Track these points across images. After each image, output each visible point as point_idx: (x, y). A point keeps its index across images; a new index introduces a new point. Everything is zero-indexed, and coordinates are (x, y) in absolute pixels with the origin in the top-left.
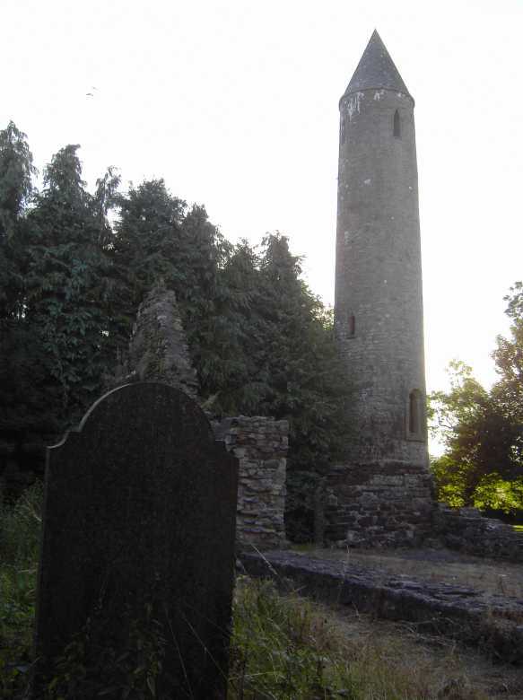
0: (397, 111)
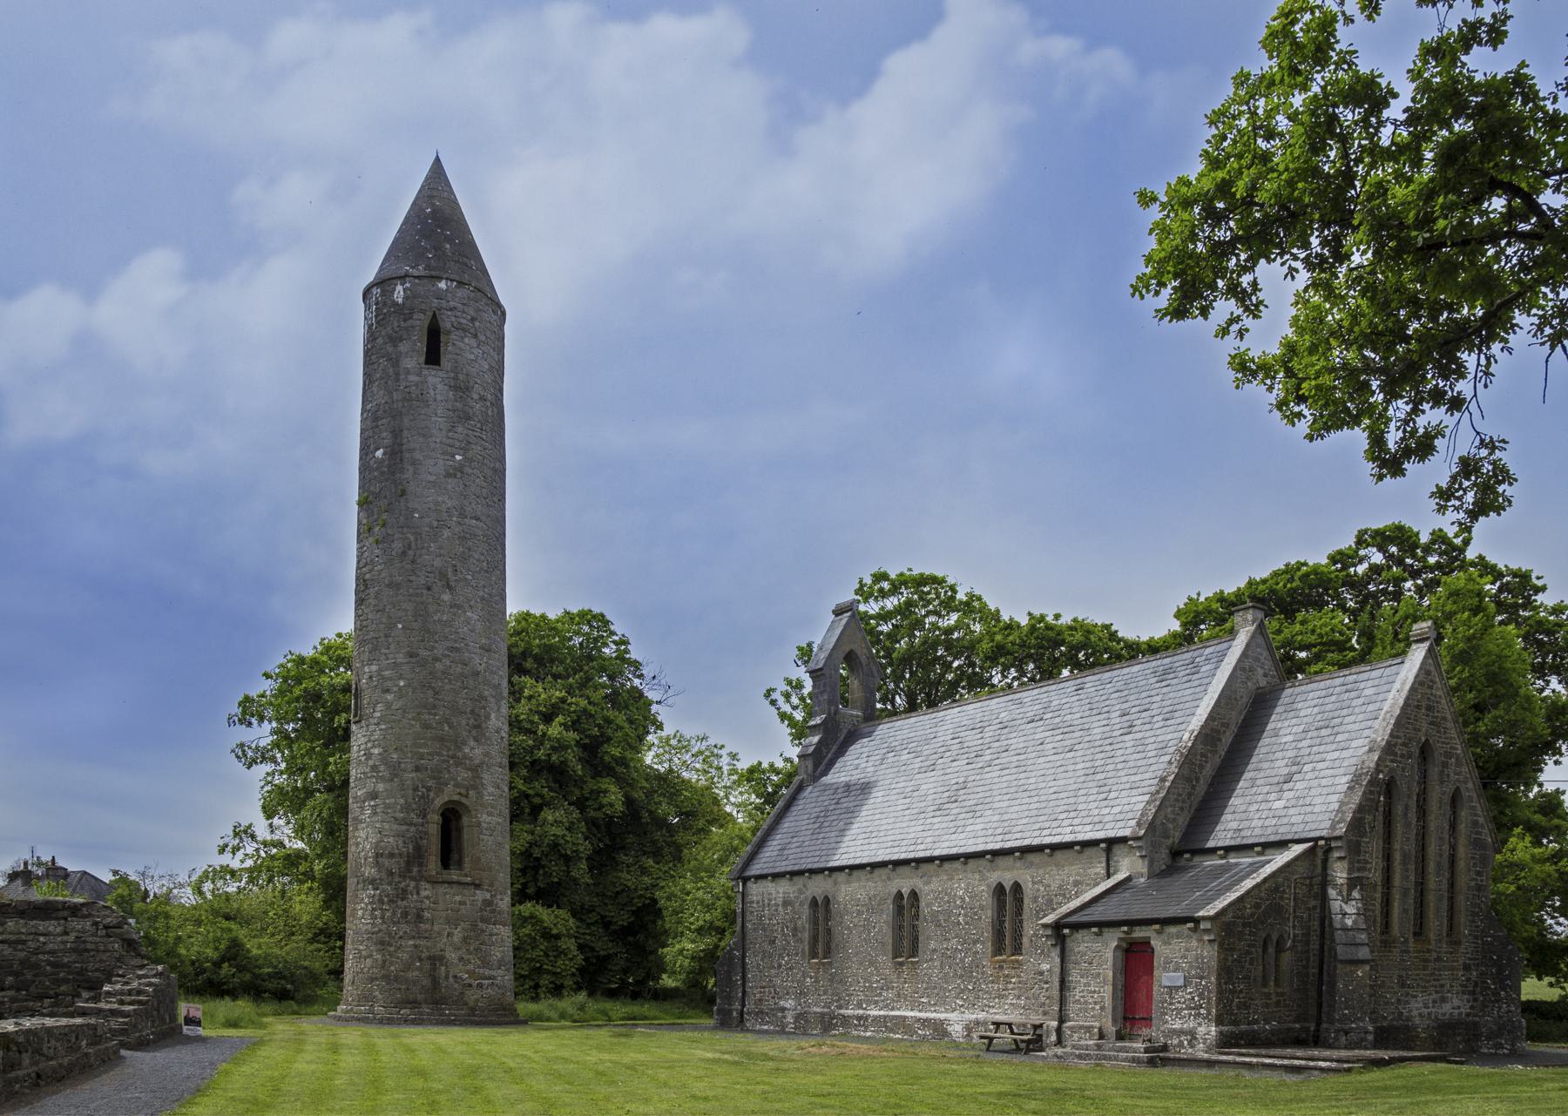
0: (434, 316)
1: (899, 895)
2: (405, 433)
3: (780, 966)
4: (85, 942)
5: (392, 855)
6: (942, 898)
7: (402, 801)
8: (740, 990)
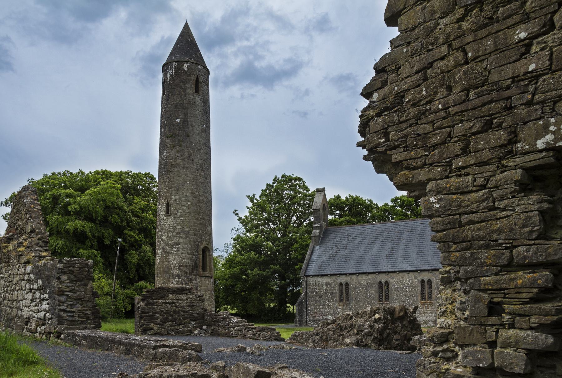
0: (197, 77)
1: (380, 282)
2: (189, 115)
3: (324, 305)
4: (193, 302)
5: (186, 266)
6: (399, 284)
7: (190, 246)
8: (305, 313)
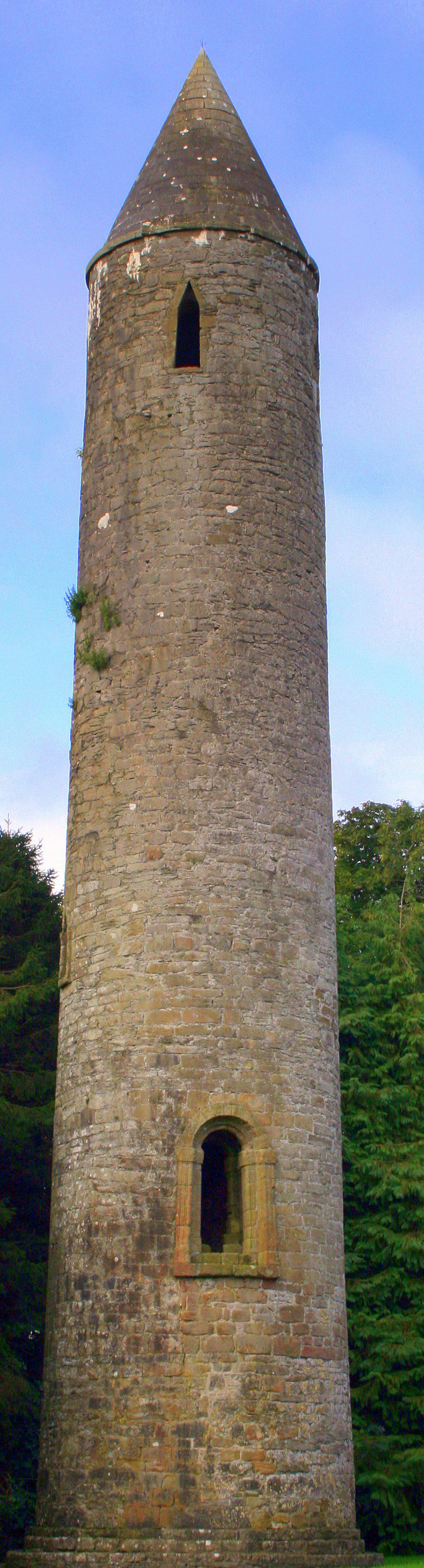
0: (189, 288)
